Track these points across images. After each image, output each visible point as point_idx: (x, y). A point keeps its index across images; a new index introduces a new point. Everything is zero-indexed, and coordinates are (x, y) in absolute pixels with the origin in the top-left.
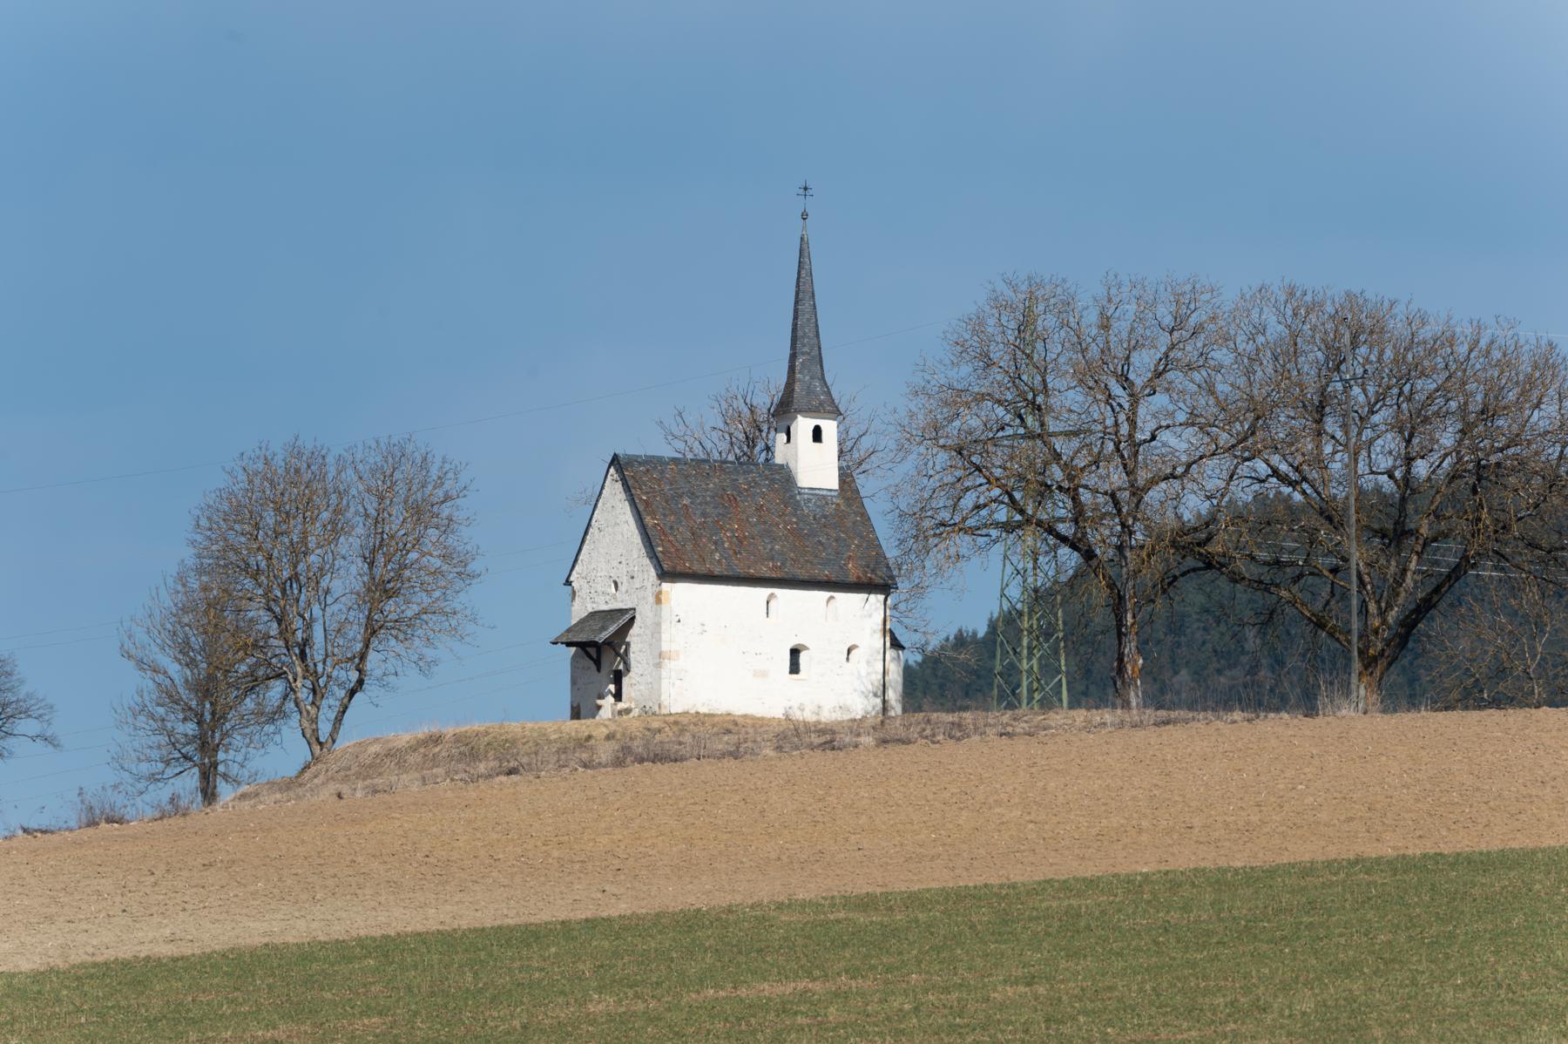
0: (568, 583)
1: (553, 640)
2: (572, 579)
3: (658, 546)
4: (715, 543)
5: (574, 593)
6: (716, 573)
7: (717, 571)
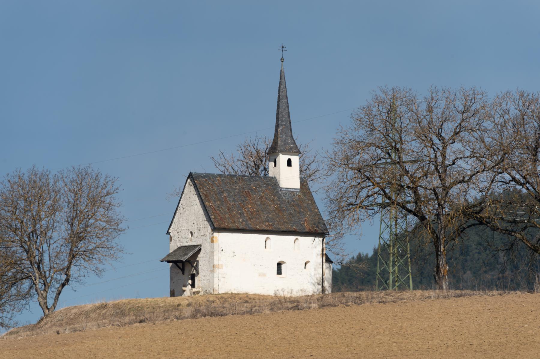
0: (168, 233)
1: (161, 259)
2: (170, 231)
3: (212, 216)
4: (240, 214)
5: (171, 238)
6: (240, 228)
7: (241, 227)
